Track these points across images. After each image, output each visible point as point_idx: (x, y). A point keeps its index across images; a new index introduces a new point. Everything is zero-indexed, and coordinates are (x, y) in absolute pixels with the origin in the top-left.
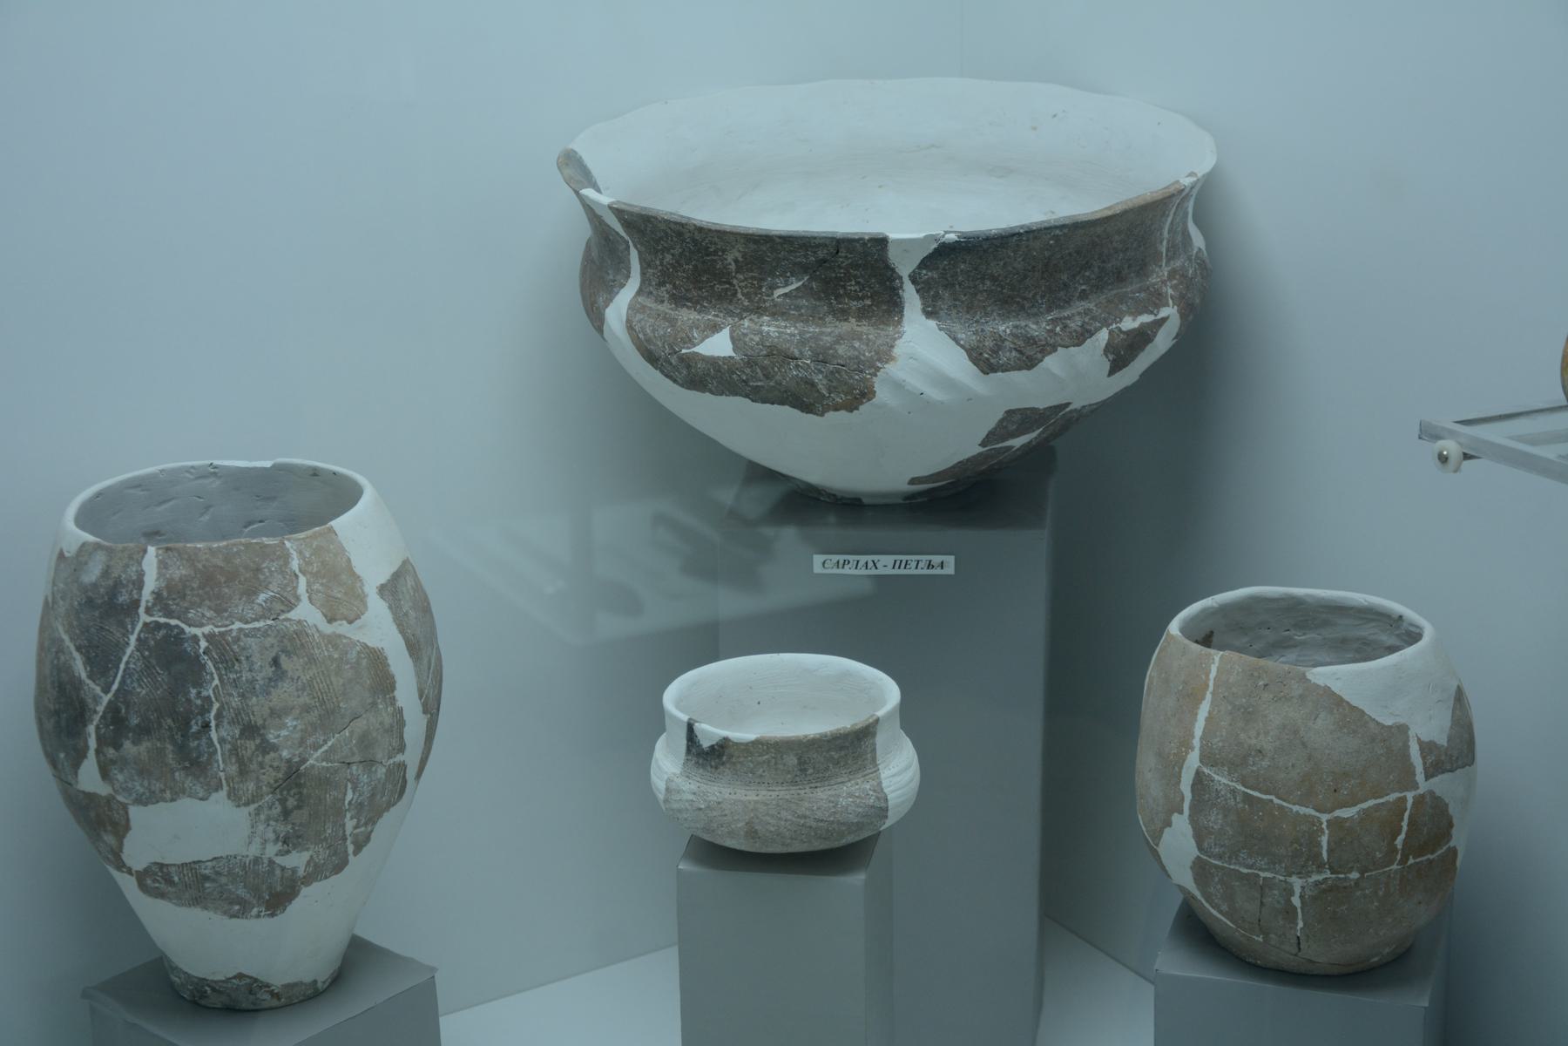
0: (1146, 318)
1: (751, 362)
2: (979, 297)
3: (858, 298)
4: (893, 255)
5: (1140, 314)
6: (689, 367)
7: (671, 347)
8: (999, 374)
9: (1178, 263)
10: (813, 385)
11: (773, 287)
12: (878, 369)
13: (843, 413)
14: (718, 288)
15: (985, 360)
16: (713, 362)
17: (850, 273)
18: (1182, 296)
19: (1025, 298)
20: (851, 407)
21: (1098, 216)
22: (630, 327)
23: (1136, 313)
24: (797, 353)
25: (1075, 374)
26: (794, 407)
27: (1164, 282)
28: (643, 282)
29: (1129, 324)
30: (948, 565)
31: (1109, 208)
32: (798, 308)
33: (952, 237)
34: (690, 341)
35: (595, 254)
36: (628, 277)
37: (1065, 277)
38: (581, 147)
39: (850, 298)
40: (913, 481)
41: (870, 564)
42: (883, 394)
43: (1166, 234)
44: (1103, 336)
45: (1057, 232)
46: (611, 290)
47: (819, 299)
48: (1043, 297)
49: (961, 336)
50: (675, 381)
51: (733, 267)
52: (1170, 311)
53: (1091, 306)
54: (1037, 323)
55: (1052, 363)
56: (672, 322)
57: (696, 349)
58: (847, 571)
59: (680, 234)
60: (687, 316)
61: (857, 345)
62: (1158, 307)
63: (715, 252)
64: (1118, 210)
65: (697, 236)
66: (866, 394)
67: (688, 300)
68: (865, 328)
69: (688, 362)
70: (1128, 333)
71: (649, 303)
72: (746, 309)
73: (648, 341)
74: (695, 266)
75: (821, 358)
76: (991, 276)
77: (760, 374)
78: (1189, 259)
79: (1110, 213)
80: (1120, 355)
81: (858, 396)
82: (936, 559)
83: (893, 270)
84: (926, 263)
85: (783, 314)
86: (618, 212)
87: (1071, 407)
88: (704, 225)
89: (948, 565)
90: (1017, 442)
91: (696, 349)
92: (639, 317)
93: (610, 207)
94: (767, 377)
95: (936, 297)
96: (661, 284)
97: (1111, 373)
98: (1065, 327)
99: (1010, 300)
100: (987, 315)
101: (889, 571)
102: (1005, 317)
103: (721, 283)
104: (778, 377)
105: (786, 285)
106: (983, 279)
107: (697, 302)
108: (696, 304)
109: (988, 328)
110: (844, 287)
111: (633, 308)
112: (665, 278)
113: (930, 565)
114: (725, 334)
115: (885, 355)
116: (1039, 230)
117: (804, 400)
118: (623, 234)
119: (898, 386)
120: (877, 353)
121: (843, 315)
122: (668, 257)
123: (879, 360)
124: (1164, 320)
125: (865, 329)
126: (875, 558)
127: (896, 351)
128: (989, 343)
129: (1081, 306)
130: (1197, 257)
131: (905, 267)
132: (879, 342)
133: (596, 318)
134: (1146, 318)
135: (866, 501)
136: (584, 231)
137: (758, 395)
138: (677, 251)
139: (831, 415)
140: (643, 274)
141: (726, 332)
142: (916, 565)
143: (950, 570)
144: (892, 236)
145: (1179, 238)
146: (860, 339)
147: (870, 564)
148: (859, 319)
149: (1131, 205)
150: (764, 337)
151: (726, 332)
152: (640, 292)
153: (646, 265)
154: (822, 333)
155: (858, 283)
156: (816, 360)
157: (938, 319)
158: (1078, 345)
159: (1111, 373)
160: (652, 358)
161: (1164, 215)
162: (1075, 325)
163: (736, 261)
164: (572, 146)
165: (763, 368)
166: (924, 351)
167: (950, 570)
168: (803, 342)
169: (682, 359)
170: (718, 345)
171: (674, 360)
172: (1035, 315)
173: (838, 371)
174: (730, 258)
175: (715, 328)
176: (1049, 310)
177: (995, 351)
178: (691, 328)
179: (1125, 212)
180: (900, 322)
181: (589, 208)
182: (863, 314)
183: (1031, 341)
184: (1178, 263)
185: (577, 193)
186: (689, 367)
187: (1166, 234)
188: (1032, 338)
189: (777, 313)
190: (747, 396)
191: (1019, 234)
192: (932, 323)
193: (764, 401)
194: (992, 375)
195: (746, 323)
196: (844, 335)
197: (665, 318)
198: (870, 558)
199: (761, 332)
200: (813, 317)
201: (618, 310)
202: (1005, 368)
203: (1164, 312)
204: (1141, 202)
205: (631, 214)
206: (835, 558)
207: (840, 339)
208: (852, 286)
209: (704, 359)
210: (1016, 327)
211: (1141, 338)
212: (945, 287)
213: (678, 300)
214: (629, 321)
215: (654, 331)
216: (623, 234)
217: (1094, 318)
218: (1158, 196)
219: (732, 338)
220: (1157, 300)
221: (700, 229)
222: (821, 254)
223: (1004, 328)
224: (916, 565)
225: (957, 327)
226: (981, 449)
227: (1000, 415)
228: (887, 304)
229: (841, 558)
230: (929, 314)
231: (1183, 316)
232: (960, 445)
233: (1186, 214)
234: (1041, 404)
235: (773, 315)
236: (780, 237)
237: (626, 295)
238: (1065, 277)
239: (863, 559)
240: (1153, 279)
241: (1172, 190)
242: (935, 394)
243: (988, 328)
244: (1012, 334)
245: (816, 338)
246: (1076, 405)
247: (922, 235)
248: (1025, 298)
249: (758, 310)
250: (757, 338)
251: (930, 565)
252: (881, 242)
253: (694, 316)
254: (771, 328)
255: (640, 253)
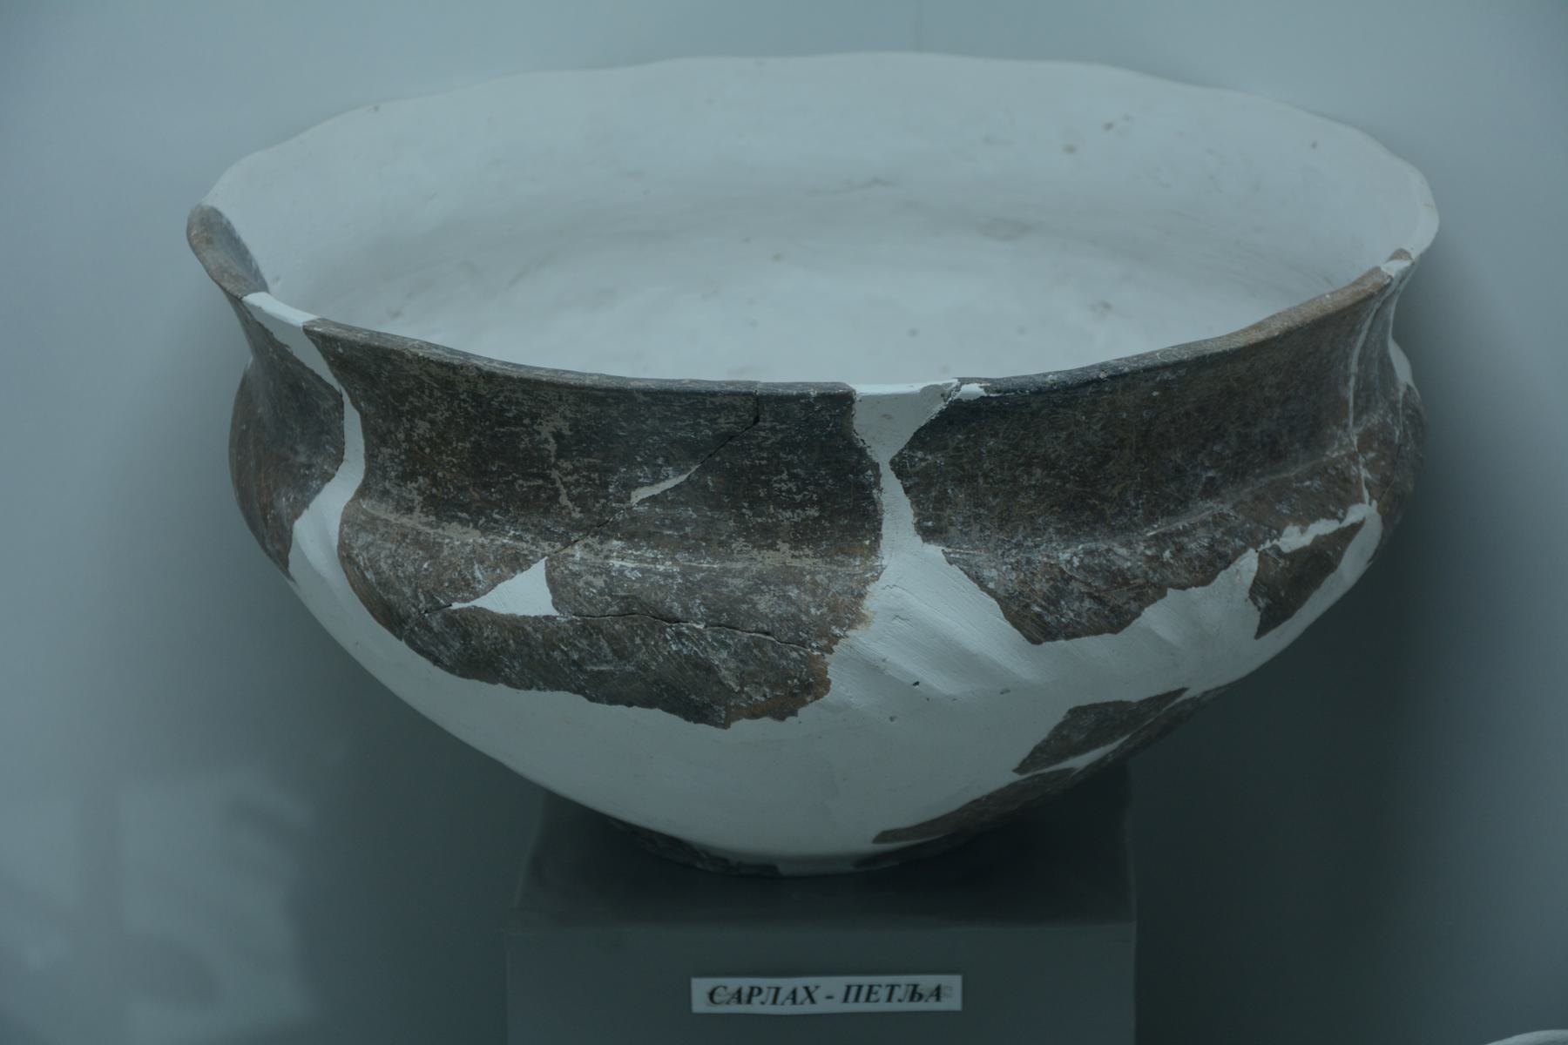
0: (1324, 527)
1: (588, 628)
2: (1023, 499)
3: (793, 506)
4: (862, 424)
5: (1314, 519)
6: (466, 636)
7: (430, 597)
8: (1062, 642)
9: (1375, 419)
10: (710, 669)
11: (630, 485)
12: (835, 639)
13: (766, 721)
14: (522, 485)
15: (1034, 619)
16: (515, 626)
17: (783, 458)
18: (1385, 482)
19: (1104, 499)
20: (782, 710)
21: (1241, 342)
22: (346, 557)
23: (1304, 521)
24: (678, 610)
25: (1196, 634)
26: (671, 710)
27: (1353, 457)
28: (370, 471)
29: (1294, 539)
30: (950, 992)
31: (1257, 327)
32: (677, 524)
33: (974, 390)
34: (468, 587)
35: (263, 410)
36: (338, 460)
37: (1177, 456)
38: (229, 198)
39: (782, 505)
40: (883, 837)
41: (801, 994)
42: (843, 685)
43: (1354, 368)
44: (1248, 564)
45: (1168, 375)
46: (306, 485)
47: (719, 507)
48: (1138, 495)
49: (989, 573)
50: (436, 661)
51: (552, 446)
52: (1364, 512)
53: (1226, 508)
54: (1128, 544)
55: (1157, 618)
56: (431, 549)
57: (480, 603)
58: (756, 1007)
59: (447, 385)
60: (460, 538)
61: (793, 593)
62: (1344, 504)
63: (518, 420)
64: (1275, 329)
65: (483, 388)
66: (812, 686)
67: (464, 507)
68: (807, 561)
69: (467, 625)
70: (1294, 556)
71: (384, 511)
72: (577, 527)
73: (385, 585)
74: (477, 444)
75: (725, 618)
76: (1050, 462)
77: (606, 649)
78: (1393, 407)
79: (1261, 336)
80: (1277, 595)
81: (794, 689)
82: (927, 982)
83: (862, 452)
84: (922, 439)
85: (649, 536)
86: (324, 342)
87: (1186, 695)
88: (496, 368)
89: (951, 992)
90: (1080, 762)
91: (480, 603)
92: (364, 538)
93: (307, 331)
94: (621, 654)
95: (942, 501)
96: (406, 477)
97: (1262, 630)
98: (1180, 549)
99: (1082, 502)
100: (1036, 531)
101: (837, 1006)
102: (1069, 535)
103: (527, 476)
104: (642, 656)
105: (656, 480)
106: (1028, 465)
107: (481, 512)
108: (477, 515)
109: (1039, 557)
110: (767, 484)
111: (349, 520)
112: (415, 465)
113: (915, 994)
114: (537, 573)
115: (848, 612)
116: (1134, 373)
117: (692, 697)
118: (329, 378)
119: (873, 670)
120: (833, 609)
121: (766, 536)
122: (423, 427)
123: (837, 622)
124: (1356, 528)
125: (807, 563)
126: (811, 981)
127: (870, 605)
128: (1041, 586)
129: (1207, 508)
130: (1406, 404)
131: (883, 452)
132: (836, 587)
133: (274, 539)
134: (1324, 527)
135: (784, 870)
136: (244, 358)
137: (601, 690)
138: (441, 415)
139: (743, 726)
140: (370, 456)
141: (538, 570)
142: (889, 994)
143: (952, 1002)
144: (862, 389)
145: (1375, 371)
146: (799, 584)
147: (801, 994)
148: (796, 544)
149: (1298, 319)
150: (615, 580)
151: (538, 570)
152: (363, 491)
153: (375, 439)
154: (726, 571)
155: (794, 477)
156: (714, 622)
157: (946, 542)
158: (1205, 582)
159: (1262, 630)
160: (390, 617)
161: (1353, 332)
162: (1197, 545)
163: (558, 436)
164: (210, 201)
165: (613, 639)
166: (922, 603)
167: (952, 1002)
168: (689, 589)
169: (452, 620)
170: (524, 595)
171: (436, 622)
172: (1124, 529)
173: (759, 644)
174: (546, 431)
175: (518, 563)
176: (1150, 519)
177: (1053, 601)
178: (469, 562)
179: (1288, 334)
180: (874, 549)
181: (259, 332)
182: (802, 536)
183: (1117, 578)
184: (1375, 419)
185: (236, 301)
186: (466, 636)
187: (1354, 368)
188: (1121, 572)
189: (636, 533)
190: (579, 691)
191: (1098, 381)
192: (935, 551)
193: (613, 700)
194: (1048, 645)
195: (578, 552)
196: (759, 572)
197: (416, 542)
198: (799, 982)
199: (607, 571)
200: (707, 540)
201: (322, 521)
202: (1072, 632)
203: (1355, 514)
204: (1314, 312)
205: (350, 345)
206: (733, 983)
207: (761, 582)
208: (782, 483)
209: (496, 620)
210: (1090, 553)
211: (1319, 560)
212: (959, 481)
213: (442, 507)
214: (342, 546)
215: (394, 566)
216: (329, 378)
217: (1230, 532)
218: (1345, 300)
219: (551, 581)
220: (1340, 492)
221: (490, 377)
222: (725, 423)
223: (1068, 555)
224: (889, 994)
225: (981, 557)
226: (1017, 777)
227: (1059, 716)
228: (847, 516)
229: (745, 983)
230: (928, 533)
231: (1386, 517)
232: (987, 768)
233: (1386, 325)
234: (1134, 695)
235: (629, 537)
236: (647, 392)
237: (335, 498)
238: (1177, 456)
239: (787, 984)
240: (1334, 453)
241: (1368, 286)
242: (940, 683)
243: (1039, 557)
244: (1082, 566)
245: (714, 581)
246: (1194, 691)
247: (917, 387)
248: (1104, 499)
249: (602, 528)
250: (599, 582)
251: (915, 994)
252: (840, 402)
253: (474, 537)
254: (625, 562)
255: (365, 418)
